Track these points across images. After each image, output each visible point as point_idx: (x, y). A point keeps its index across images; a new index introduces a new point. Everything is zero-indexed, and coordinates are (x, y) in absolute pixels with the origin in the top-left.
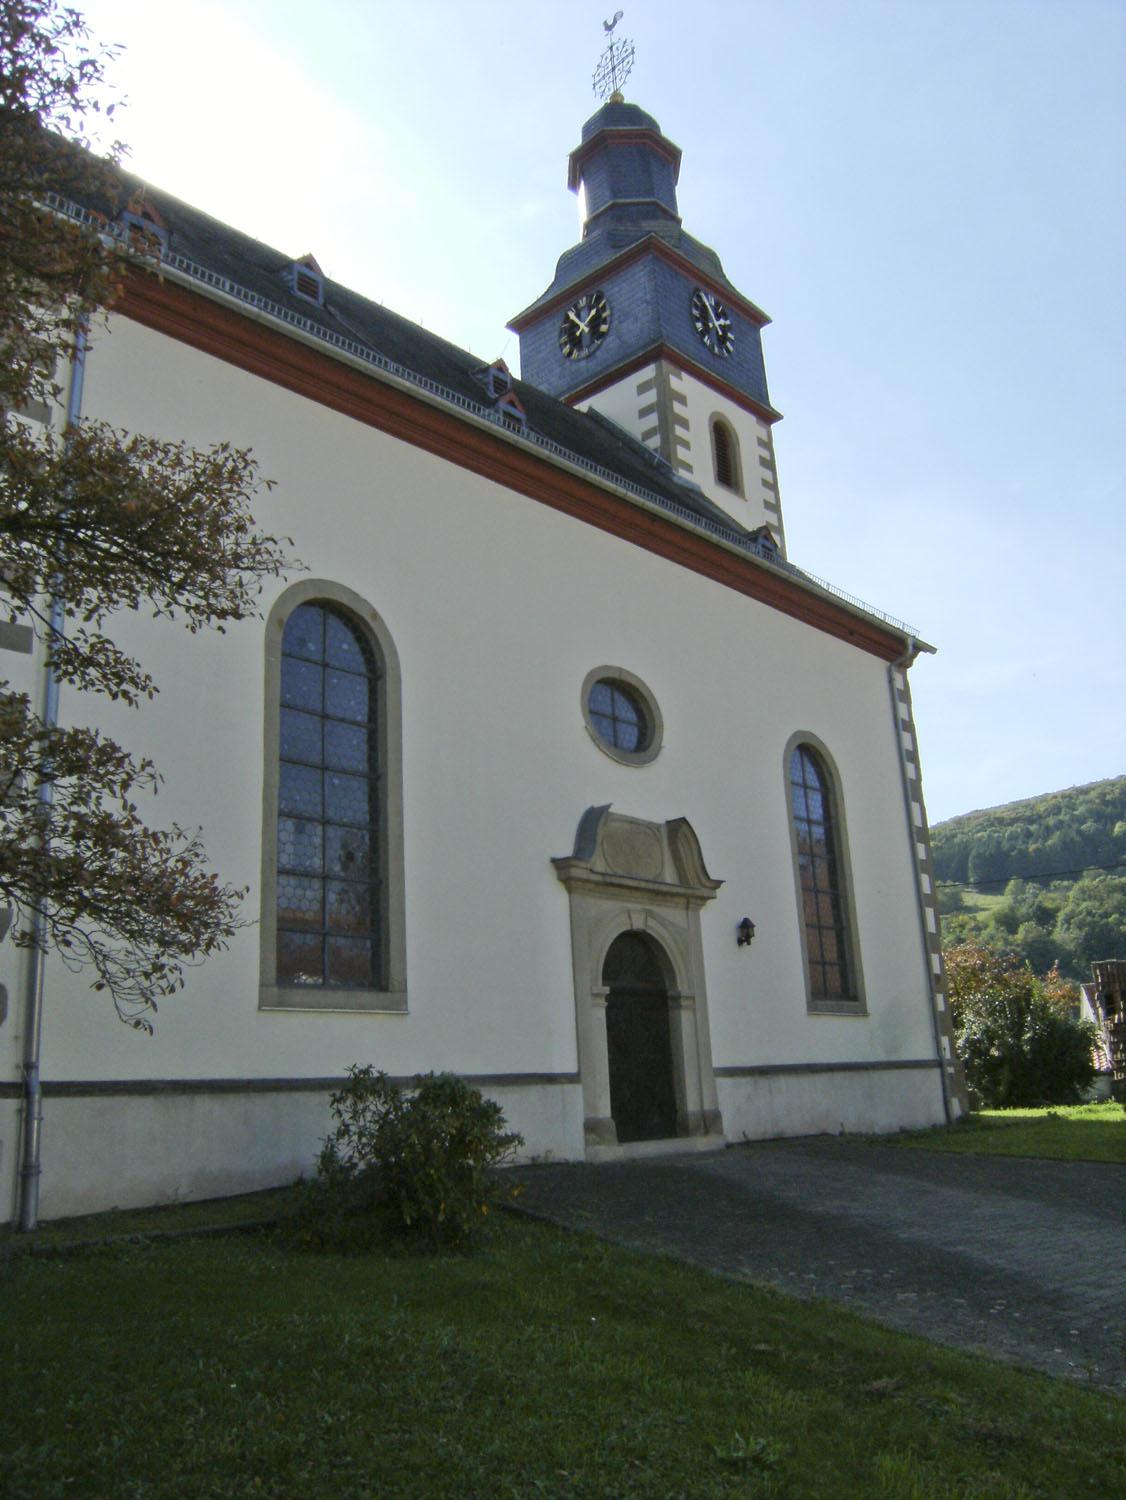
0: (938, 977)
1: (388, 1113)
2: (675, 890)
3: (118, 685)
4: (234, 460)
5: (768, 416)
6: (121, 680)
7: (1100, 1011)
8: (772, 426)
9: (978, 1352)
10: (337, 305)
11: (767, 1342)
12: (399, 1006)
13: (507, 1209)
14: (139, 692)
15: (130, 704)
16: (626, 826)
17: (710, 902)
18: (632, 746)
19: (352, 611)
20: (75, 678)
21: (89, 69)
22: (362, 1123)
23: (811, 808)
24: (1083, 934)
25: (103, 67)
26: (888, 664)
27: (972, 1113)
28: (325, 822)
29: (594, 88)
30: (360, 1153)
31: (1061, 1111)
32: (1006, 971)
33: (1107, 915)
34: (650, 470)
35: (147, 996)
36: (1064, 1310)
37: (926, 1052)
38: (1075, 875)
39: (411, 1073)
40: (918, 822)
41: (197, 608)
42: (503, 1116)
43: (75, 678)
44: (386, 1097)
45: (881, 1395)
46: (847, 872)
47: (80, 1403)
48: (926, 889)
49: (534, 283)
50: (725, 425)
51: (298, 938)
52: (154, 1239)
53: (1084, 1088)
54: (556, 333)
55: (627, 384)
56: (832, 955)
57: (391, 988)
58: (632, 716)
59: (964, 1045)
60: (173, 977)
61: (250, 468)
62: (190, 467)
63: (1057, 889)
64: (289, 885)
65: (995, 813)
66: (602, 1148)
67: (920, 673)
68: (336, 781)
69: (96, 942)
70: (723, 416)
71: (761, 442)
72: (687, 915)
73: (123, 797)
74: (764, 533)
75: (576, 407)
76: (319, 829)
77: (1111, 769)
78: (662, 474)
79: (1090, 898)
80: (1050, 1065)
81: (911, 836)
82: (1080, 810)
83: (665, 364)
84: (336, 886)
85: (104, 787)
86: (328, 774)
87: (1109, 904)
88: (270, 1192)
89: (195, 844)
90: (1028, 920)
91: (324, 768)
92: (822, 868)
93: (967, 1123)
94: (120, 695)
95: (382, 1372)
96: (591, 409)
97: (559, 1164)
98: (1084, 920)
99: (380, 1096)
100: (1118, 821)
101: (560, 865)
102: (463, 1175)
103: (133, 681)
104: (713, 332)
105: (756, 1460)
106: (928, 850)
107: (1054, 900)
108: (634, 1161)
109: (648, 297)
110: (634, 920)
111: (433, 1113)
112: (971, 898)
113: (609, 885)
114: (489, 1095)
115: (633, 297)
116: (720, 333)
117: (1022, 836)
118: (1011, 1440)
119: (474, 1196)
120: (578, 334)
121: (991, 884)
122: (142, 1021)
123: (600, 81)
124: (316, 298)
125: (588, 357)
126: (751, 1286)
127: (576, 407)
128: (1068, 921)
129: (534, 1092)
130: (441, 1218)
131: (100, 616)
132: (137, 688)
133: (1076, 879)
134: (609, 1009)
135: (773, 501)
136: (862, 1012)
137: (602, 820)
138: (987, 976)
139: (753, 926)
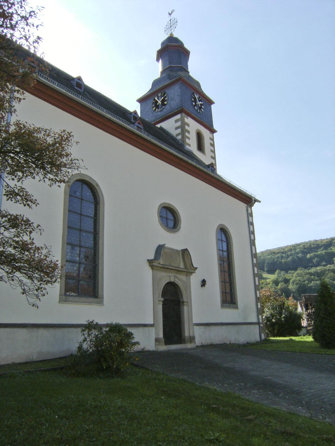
0: (258, 298)
1: (98, 335)
2: (184, 270)
3: (26, 202)
4: (66, 135)
5: (213, 131)
6: (27, 200)
7: (304, 309)
8: (214, 134)
9: (278, 408)
10: (87, 91)
11: (216, 404)
12: (101, 303)
13: (133, 364)
14: (33, 204)
15: (30, 208)
16: (170, 251)
17: (193, 274)
18: (172, 227)
19: (90, 183)
20: (13, 199)
21: (32, 14)
22: (91, 338)
23: (223, 247)
24: (297, 287)
25: (37, 13)
26: (247, 205)
27: (267, 338)
28: (80, 247)
29: (165, 32)
30: (90, 346)
31: (293, 338)
32: (277, 297)
33: (304, 281)
34: (179, 146)
35: (37, 297)
36: (300, 396)
37: (255, 320)
38: (295, 269)
39: (105, 323)
40: (254, 252)
41: (52, 179)
42: (134, 336)
43: (13, 199)
44: (98, 330)
45: (250, 421)
46: (233, 266)
47: (9, 422)
48: (256, 272)
49: (145, 89)
50: (200, 133)
51: (71, 281)
52: (26, 372)
53: (299, 332)
54: (151, 104)
55: (171, 119)
56: (228, 290)
57: (99, 297)
58: (172, 218)
59: (265, 318)
60: (44, 291)
61: (71, 138)
62: (53, 136)
63: (290, 273)
64: (69, 265)
65: (273, 250)
66: (160, 346)
67: (256, 208)
68: (84, 234)
69: (21, 280)
70: (200, 130)
71: (211, 139)
72: (187, 277)
73: (30, 236)
74: (212, 165)
75: (157, 126)
76: (78, 249)
77: (326, 233)
78: (182, 147)
79: (300, 276)
80: (291, 325)
81: (252, 256)
82: (298, 250)
83: (183, 114)
84: (83, 266)
85: (24, 233)
86: (82, 232)
87: (305, 278)
88: (61, 358)
89: (49, 251)
90: (282, 282)
91: (81, 230)
92: (226, 264)
93: (266, 341)
94: (26, 205)
95: (101, 413)
96: (161, 127)
97: (147, 351)
98: (298, 282)
99: (96, 330)
100: (308, 254)
101: (150, 261)
102: (121, 354)
103: (31, 201)
104: (198, 106)
105: (217, 439)
106: (257, 261)
107: (289, 276)
108: (169, 350)
109: (179, 94)
110: (171, 279)
111: (113, 335)
112: (265, 275)
113: (164, 268)
114: (129, 330)
115: (175, 94)
116: (200, 106)
117: (280, 258)
118: (291, 434)
119: (125, 360)
120: (158, 104)
121: (271, 271)
122: (35, 304)
123: (167, 30)
124: (81, 89)
125: (160, 111)
126: (208, 388)
127: (157, 126)
128: (293, 283)
129: (141, 329)
130: (115, 366)
131: (23, 181)
132: (32, 203)
133: (296, 271)
134: (163, 305)
135: (214, 156)
136: (237, 308)
137: (163, 248)
138: (272, 298)
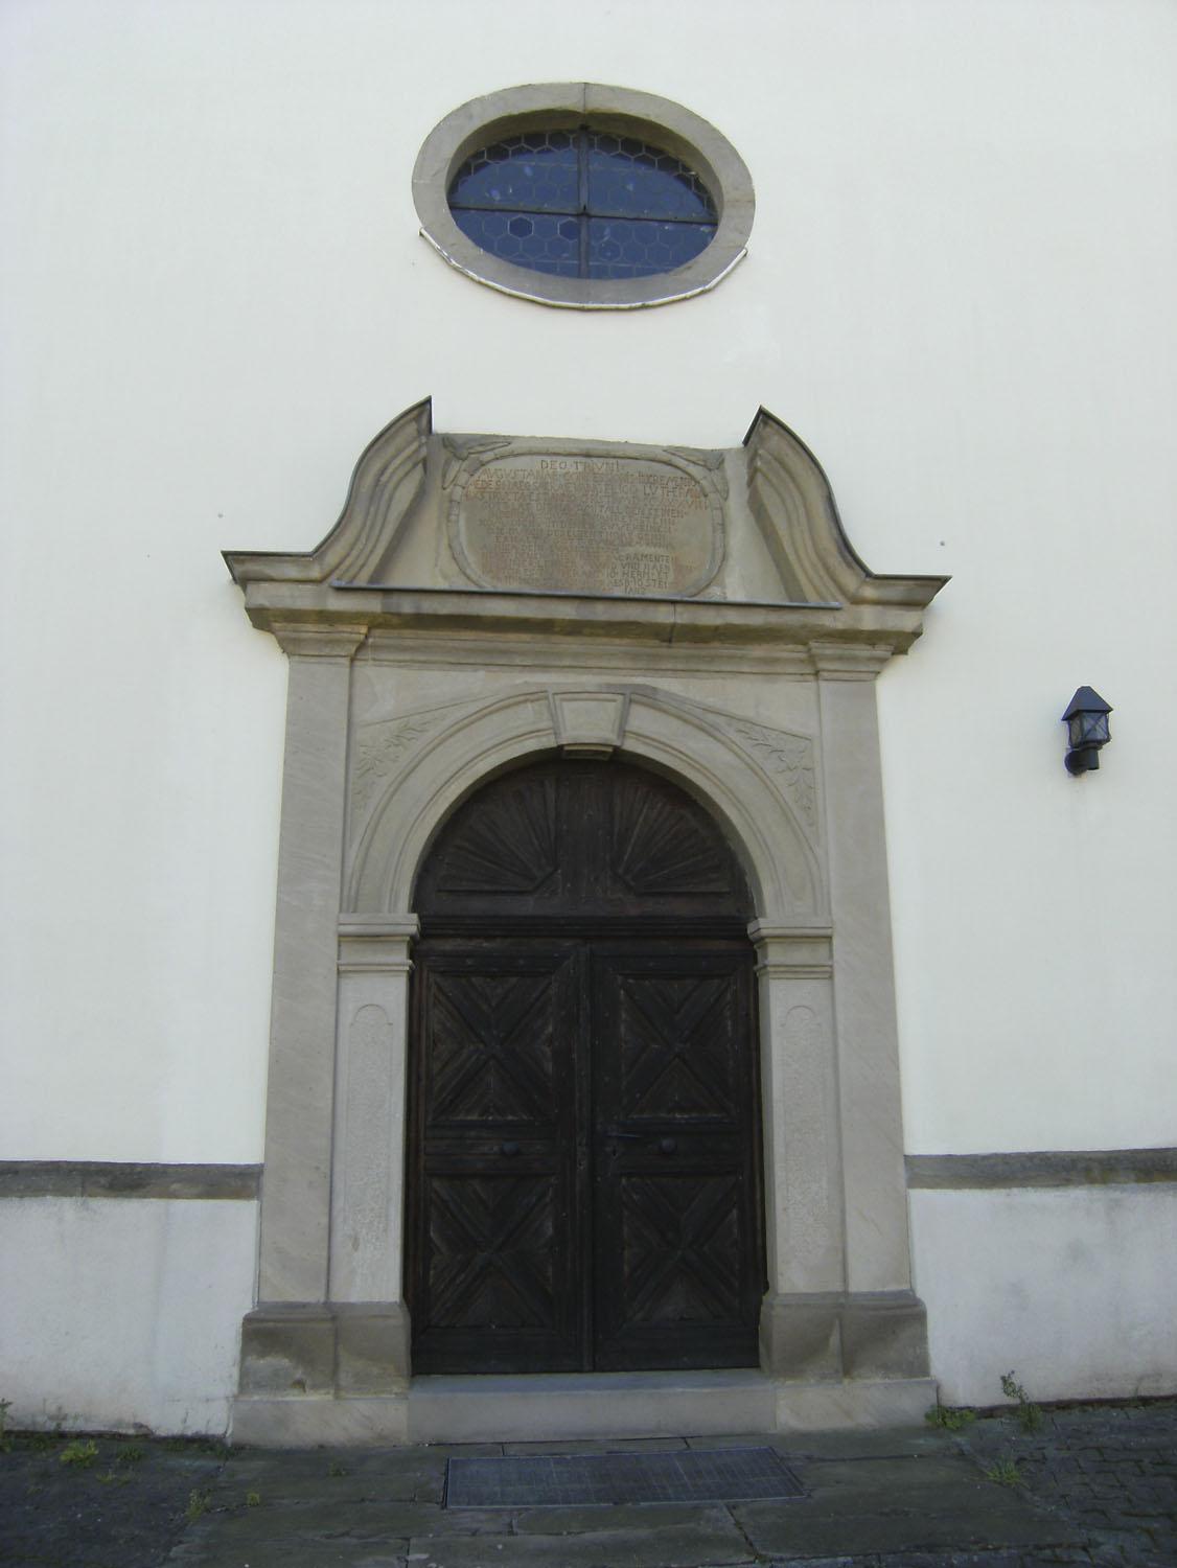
16: (571, 466)
139: (1104, 710)
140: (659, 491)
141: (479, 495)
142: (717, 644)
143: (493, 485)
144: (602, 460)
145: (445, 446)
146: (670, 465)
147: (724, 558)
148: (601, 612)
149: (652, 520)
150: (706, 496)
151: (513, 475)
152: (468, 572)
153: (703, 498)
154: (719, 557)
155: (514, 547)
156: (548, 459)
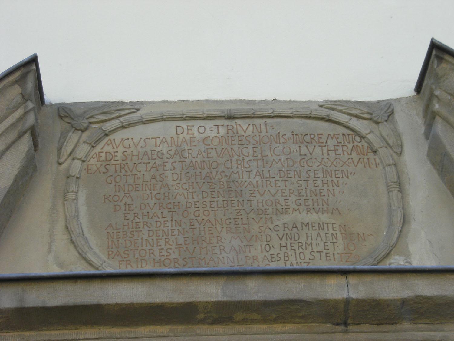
140: (318, 150)
141: (103, 169)
142: (406, 325)
143: (119, 155)
144: (248, 121)
145: (61, 117)
146: (328, 121)
147: (405, 221)
148: (254, 290)
149: (310, 183)
150: (375, 152)
151: (142, 143)
152: (90, 256)
153: (371, 155)
154: (398, 218)
155: (145, 224)
156: (184, 124)
